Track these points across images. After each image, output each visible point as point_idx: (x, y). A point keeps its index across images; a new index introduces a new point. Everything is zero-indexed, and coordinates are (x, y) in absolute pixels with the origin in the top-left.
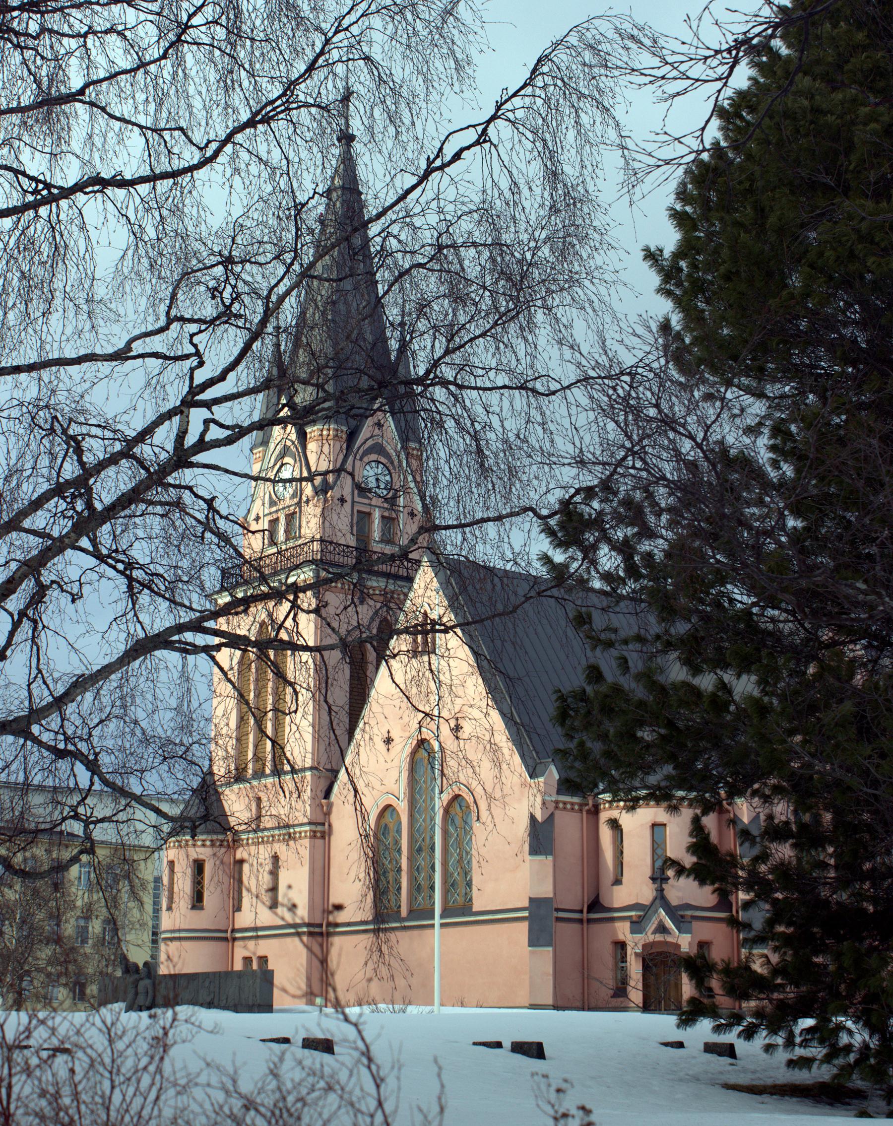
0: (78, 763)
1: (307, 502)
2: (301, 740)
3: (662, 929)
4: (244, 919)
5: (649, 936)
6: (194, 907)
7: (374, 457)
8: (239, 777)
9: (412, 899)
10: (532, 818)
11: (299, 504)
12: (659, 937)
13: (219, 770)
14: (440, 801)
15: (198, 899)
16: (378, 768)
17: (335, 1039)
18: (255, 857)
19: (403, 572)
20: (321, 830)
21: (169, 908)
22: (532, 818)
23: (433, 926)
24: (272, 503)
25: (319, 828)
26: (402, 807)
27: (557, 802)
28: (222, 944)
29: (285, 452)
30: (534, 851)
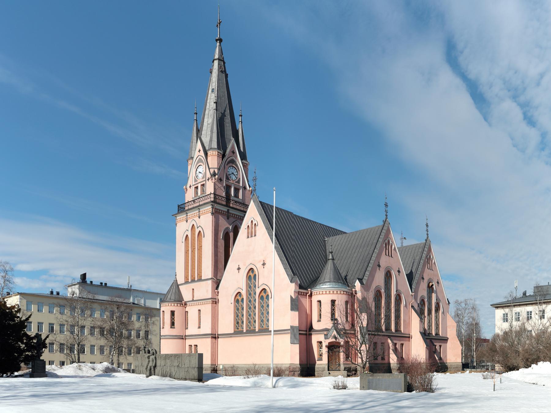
0: (220, 217)
1: (208, 180)
2: (207, 271)
3: (336, 338)
4: (188, 332)
5: (331, 340)
6: (171, 327)
7: (231, 164)
8: (187, 282)
9: (260, 325)
10: (291, 297)
11: (205, 180)
12: (334, 340)
13: (181, 279)
14: (258, 291)
15: (173, 324)
16: (233, 280)
17: (58, 353)
18: (192, 311)
19: (242, 209)
20: (215, 302)
21: (163, 328)
22: (291, 297)
23: (271, 334)
24: (196, 181)
25: (214, 300)
26: (244, 293)
27: (299, 292)
28: (180, 341)
29: (200, 161)
30: (292, 309)
